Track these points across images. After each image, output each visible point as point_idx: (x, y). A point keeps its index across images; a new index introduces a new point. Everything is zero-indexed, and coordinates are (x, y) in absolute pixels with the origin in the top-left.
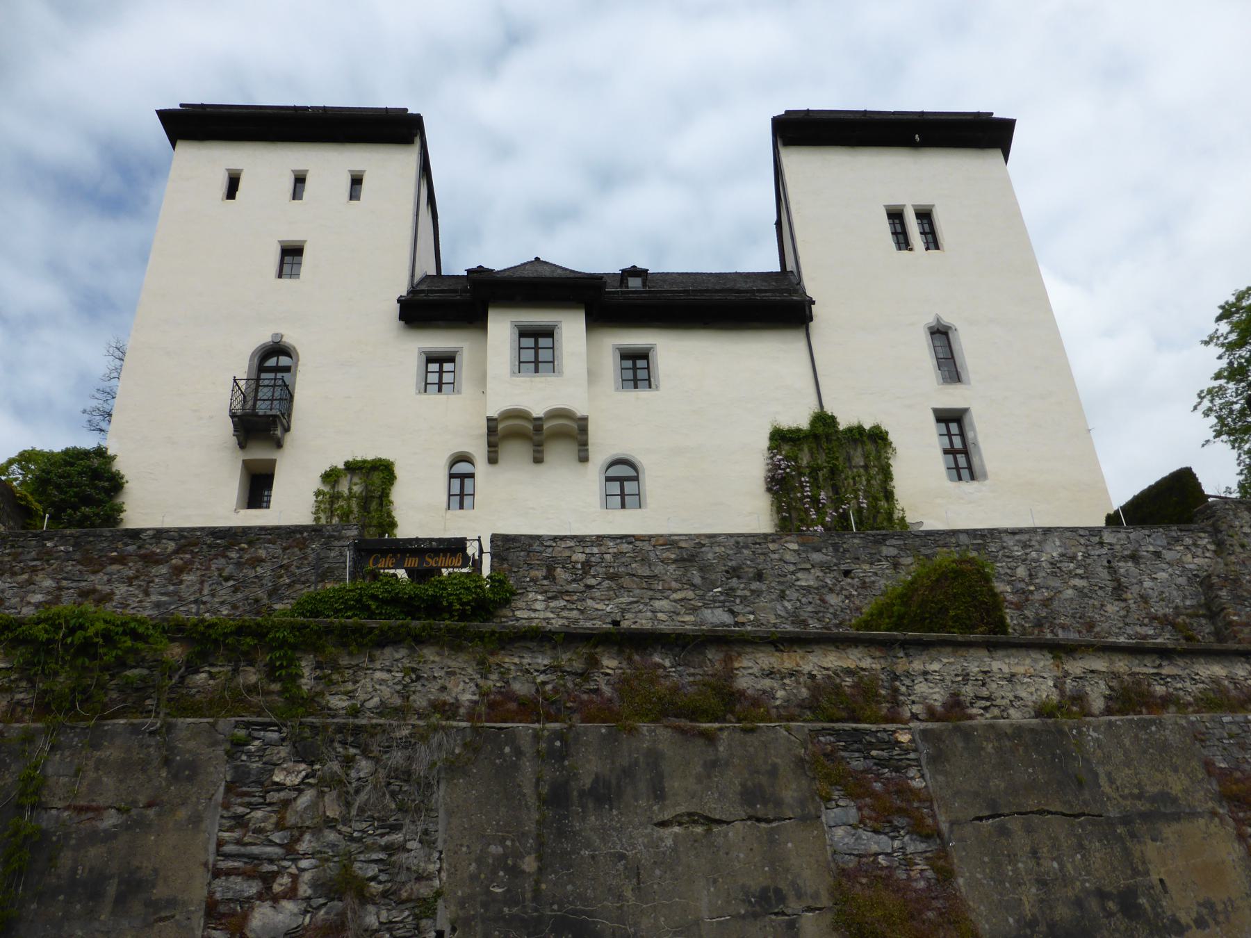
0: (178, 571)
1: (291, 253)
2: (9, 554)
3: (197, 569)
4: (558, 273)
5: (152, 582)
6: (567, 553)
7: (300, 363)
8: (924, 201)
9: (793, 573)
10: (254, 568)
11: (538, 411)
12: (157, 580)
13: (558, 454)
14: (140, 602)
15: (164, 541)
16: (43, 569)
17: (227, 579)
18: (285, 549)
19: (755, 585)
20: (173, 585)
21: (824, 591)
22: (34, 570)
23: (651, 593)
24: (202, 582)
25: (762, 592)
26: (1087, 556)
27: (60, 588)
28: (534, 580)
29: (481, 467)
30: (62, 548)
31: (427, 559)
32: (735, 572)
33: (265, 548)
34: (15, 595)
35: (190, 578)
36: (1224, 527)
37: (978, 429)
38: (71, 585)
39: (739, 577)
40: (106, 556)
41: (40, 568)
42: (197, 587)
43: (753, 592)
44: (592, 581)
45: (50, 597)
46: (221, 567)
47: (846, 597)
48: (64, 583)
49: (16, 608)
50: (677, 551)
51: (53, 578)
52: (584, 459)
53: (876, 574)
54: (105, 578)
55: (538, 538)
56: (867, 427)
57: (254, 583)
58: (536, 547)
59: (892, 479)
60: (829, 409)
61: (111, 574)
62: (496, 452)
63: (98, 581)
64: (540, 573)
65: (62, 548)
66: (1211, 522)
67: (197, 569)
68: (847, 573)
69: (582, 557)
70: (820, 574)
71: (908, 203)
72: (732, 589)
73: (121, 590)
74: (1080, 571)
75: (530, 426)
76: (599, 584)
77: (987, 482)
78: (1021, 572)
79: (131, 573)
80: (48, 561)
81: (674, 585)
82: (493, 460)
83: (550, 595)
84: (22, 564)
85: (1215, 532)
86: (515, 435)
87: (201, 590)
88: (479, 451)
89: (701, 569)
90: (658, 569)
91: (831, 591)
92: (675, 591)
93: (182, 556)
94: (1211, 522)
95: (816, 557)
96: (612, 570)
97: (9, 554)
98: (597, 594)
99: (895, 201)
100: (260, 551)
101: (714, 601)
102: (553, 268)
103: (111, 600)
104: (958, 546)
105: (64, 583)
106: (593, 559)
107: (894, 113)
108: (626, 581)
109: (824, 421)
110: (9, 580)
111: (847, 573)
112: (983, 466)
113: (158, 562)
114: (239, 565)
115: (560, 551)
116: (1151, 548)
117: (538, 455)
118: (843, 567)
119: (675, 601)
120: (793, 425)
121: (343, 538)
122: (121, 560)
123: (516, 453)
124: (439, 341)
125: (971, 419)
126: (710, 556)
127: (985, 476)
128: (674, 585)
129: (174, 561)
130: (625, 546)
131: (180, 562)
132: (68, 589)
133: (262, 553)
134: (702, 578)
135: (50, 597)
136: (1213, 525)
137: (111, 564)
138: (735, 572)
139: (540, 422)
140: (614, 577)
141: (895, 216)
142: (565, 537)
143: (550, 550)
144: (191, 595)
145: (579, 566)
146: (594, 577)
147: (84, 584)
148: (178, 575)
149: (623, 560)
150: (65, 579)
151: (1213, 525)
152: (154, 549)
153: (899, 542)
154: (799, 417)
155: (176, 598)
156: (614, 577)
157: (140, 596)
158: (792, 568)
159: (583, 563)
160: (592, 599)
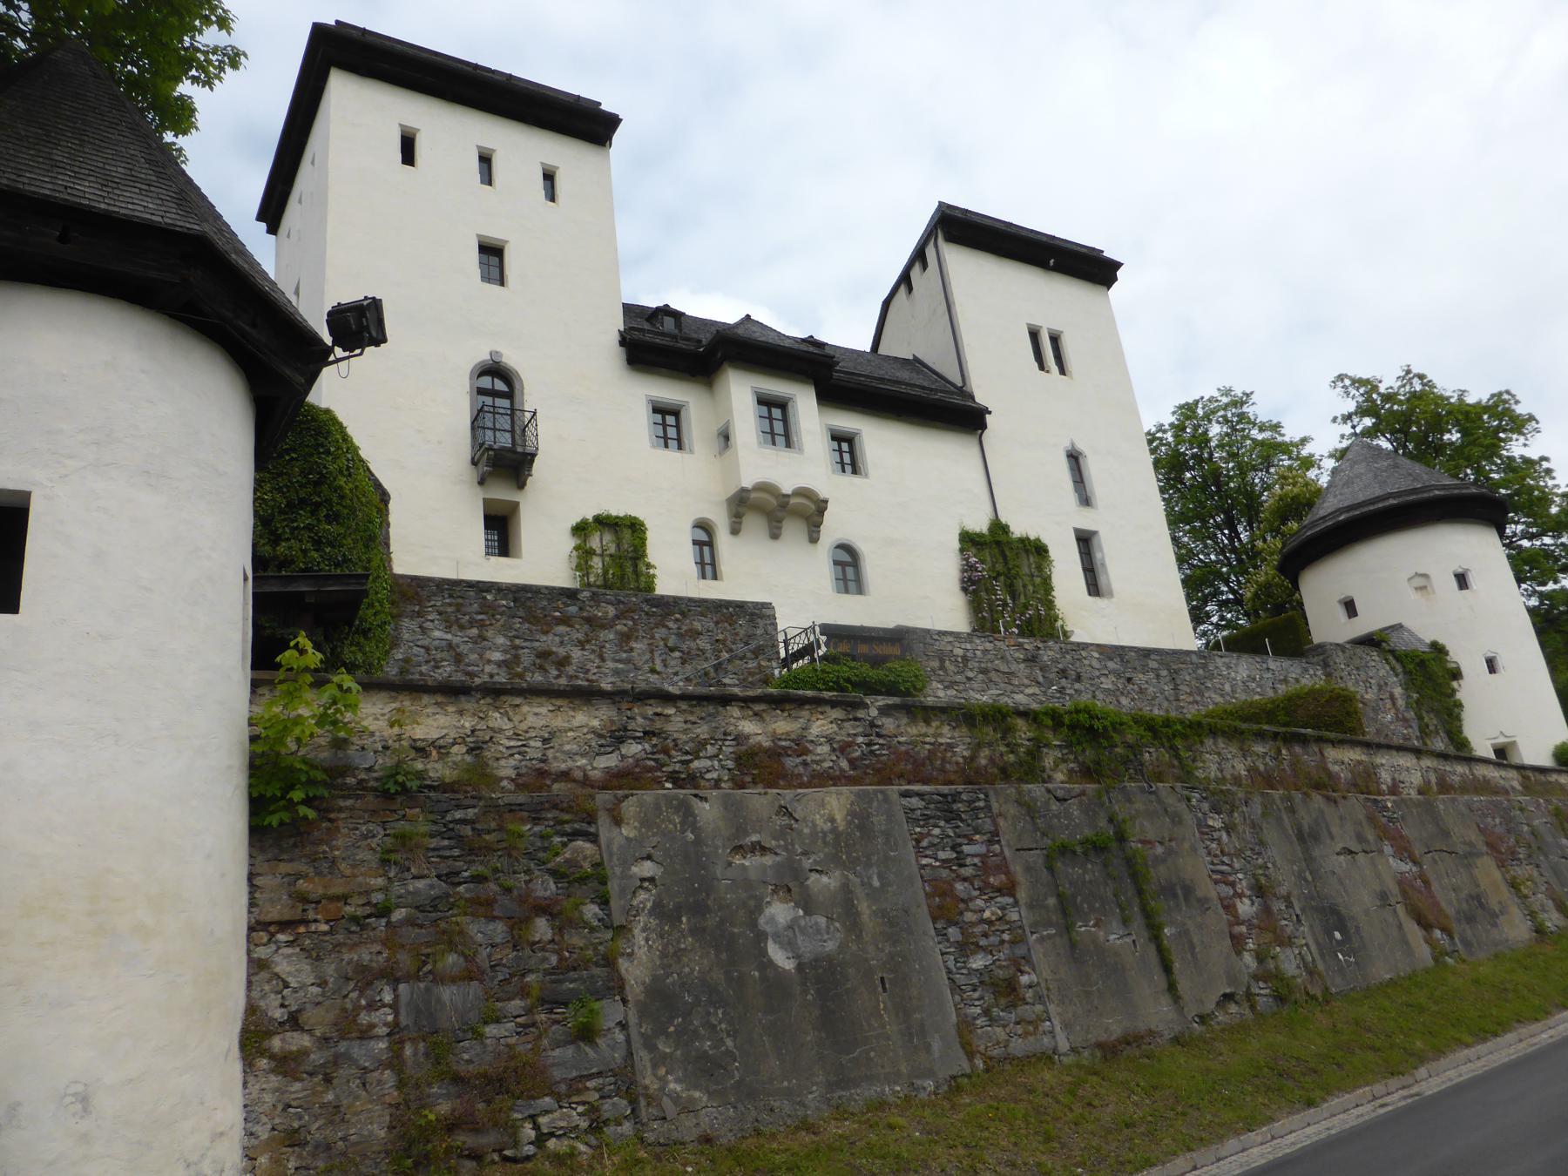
0: (626, 638)
1: (492, 252)
2: (450, 605)
3: (643, 637)
4: (770, 339)
5: (604, 647)
6: (950, 648)
7: (525, 391)
8: (1056, 327)
9: (1098, 677)
10: (695, 640)
11: (787, 488)
12: (607, 645)
13: (794, 531)
14: (598, 667)
15: (603, 604)
16: (491, 625)
17: (672, 650)
18: (717, 623)
19: (1077, 686)
20: (625, 652)
21: (1118, 693)
22: (482, 625)
23: (1012, 687)
24: (652, 652)
25: (1081, 692)
26: (1261, 678)
27: (516, 648)
28: (933, 670)
29: (723, 539)
30: (504, 602)
31: (875, 647)
32: (1063, 673)
33: (699, 620)
34: (472, 651)
35: (638, 646)
36: (1331, 663)
37: (1105, 551)
38: (525, 644)
39: (1066, 678)
40: (550, 615)
41: (488, 623)
42: (648, 656)
43: (1076, 690)
44: (970, 674)
45: (508, 656)
46: (664, 636)
47: (1132, 700)
48: (517, 642)
49: (478, 666)
50: (1023, 652)
51: (505, 636)
52: (814, 539)
53: (1147, 682)
54: (557, 639)
55: (928, 631)
56: (1032, 538)
57: (698, 655)
58: (928, 640)
59: (1447, 653)
60: (1003, 520)
61: (561, 636)
62: (740, 523)
63: (548, 641)
64: (936, 664)
65: (504, 602)
66: (1321, 658)
67: (643, 637)
68: (1129, 680)
69: (959, 652)
70: (1114, 679)
71: (1046, 325)
72: (1063, 688)
73: (576, 654)
74: (1259, 690)
75: (774, 502)
76: (975, 677)
77: (1114, 600)
78: (1227, 687)
79: (580, 636)
80: (493, 615)
81: (1026, 682)
82: (735, 531)
83: (946, 684)
84: (467, 617)
85: (1326, 665)
86: (759, 508)
87: (653, 660)
88: (721, 521)
89: (1041, 670)
90: (1014, 667)
91: (1122, 693)
92: (1027, 686)
93: (625, 622)
94: (1321, 658)
95: (1111, 665)
96: (983, 665)
97: (450, 605)
98: (975, 686)
99: (1036, 322)
100: (695, 623)
101: (1053, 697)
102: (855, 355)
103: (569, 664)
104: (1192, 663)
105: (517, 642)
106: (968, 654)
107: (1032, 231)
108: (993, 675)
109: (998, 527)
110: (459, 634)
111: (1129, 680)
112: (1109, 585)
113: (603, 627)
114: (680, 636)
115: (943, 645)
116: (1294, 676)
117: (776, 531)
118: (1128, 675)
119: (1028, 695)
120: (978, 530)
121: (764, 616)
122: (566, 621)
123: (754, 524)
124: (669, 391)
125: (1099, 541)
126: (1046, 658)
127: (1110, 594)
128: (1026, 682)
129: (618, 627)
130: (988, 644)
131: (625, 629)
132: (523, 648)
133: (697, 626)
134: (1044, 677)
135: (508, 656)
136: (1323, 661)
137: (558, 624)
138: (1063, 673)
139: (786, 499)
140: (984, 671)
141: (1034, 335)
142: (946, 632)
143: (937, 643)
144: (645, 663)
145: (960, 660)
146: (971, 670)
147: (537, 644)
148: (627, 643)
149: (989, 657)
150: (518, 637)
151: (1323, 661)
152: (596, 612)
153: (1158, 658)
154: (979, 523)
155: (631, 666)
156: (984, 671)
157: (597, 661)
158: (1097, 673)
159: (962, 657)
160: (973, 690)
